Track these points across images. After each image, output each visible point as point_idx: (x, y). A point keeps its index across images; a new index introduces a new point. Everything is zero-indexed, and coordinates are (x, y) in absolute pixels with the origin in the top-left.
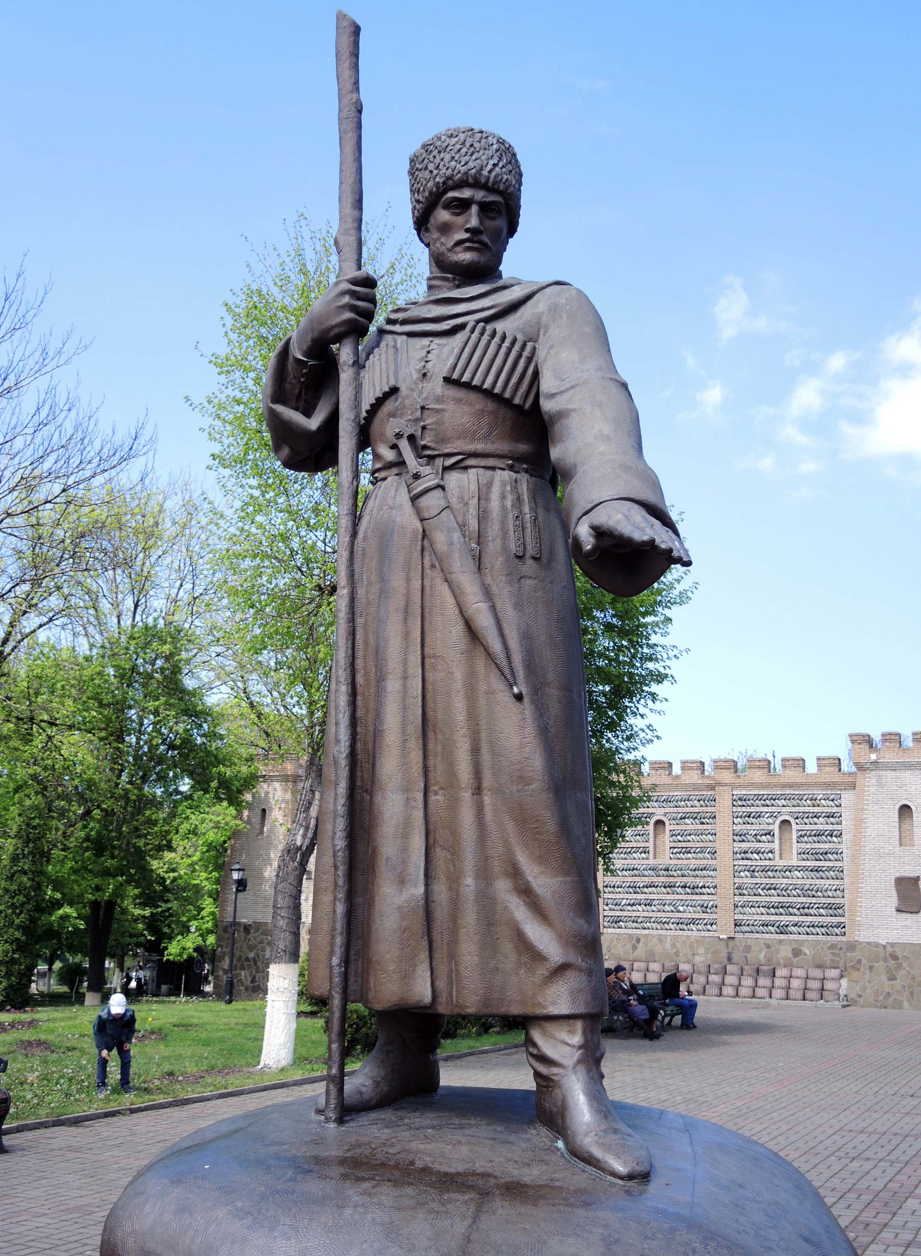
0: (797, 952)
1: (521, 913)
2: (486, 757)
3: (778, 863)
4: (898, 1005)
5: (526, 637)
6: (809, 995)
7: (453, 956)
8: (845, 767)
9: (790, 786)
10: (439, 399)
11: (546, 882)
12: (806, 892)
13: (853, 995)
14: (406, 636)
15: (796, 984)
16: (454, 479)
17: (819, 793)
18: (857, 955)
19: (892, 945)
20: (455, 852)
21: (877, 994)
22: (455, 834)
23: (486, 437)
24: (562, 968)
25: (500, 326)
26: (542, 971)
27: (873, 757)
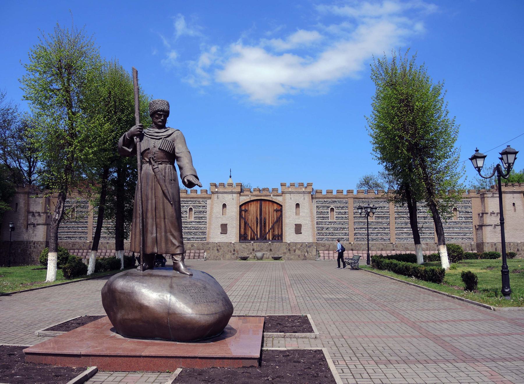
0: (192, 246)
1: (172, 238)
2: (166, 214)
3: (188, 220)
4: (220, 259)
5: (173, 194)
6: (195, 258)
7: (161, 245)
8: (208, 192)
9: (193, 198)
10: (157, 152)
11: (176, 234)
12: (196, 228)
13: (207, 257)
14: (152, 193)
15: (192, 254)
16: (160, 166)
17: (201, 200)
18: (209, 246)
19: (219, 243)
20: (161, 229)
21: (214, 256)
22: (161, 225)
23: (165, 159)
24: (178, 247)
25: (168, 139)
26: (175, 247)
27: (216, 190)
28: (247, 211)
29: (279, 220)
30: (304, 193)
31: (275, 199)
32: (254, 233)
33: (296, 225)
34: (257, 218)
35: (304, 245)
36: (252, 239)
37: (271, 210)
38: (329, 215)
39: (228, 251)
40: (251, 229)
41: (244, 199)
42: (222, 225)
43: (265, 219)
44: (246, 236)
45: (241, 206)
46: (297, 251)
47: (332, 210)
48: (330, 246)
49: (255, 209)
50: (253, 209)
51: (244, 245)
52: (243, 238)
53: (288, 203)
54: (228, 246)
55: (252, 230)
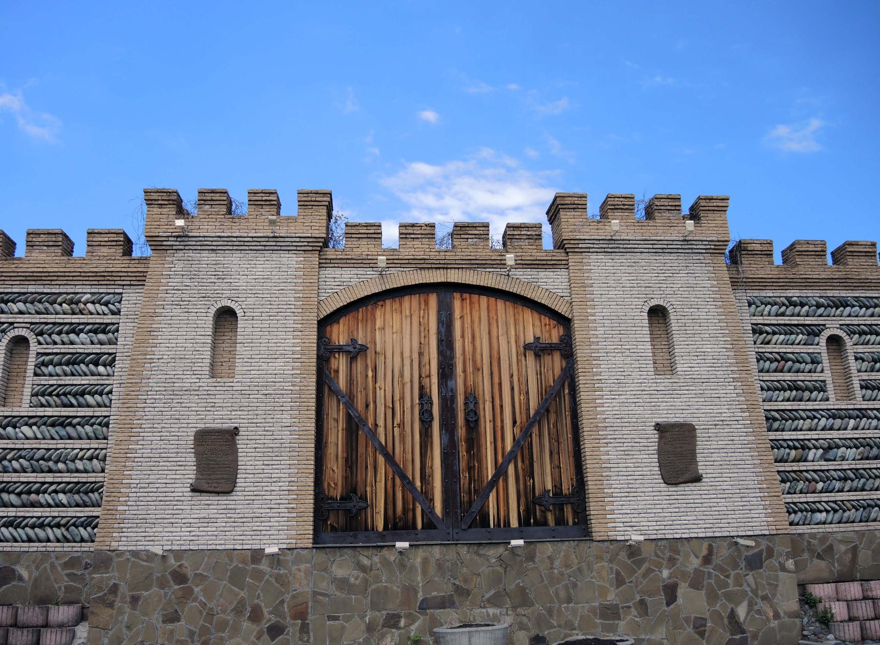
12: (38, 462)
17: (86, 291)
18: (112, 576)
19: (179, 554)
28: (363, 349)
29: (562, 401)
30: (687, 246)
31: (522, 282)
32: (408, 484)
33: (658, 427)
34: (424, 395)
35: (723, 552)
36: (398, 526)
37: (508, 350)
38: (827, 376)
39: (238, 611)
40: (390, 459)
41: (346, 284)
42: (203, 437)
43: (472, 399)
44: (354, 504)
45: (325, 323)
46: (683, 590)
47: (834, 341)
48: (854, 550)
49: (409, 344)
50: (401, 339)
51: (342, 567)
52: (338, 517)
53: (607, 300)
54: (236, 577)
55: (398, 471)
